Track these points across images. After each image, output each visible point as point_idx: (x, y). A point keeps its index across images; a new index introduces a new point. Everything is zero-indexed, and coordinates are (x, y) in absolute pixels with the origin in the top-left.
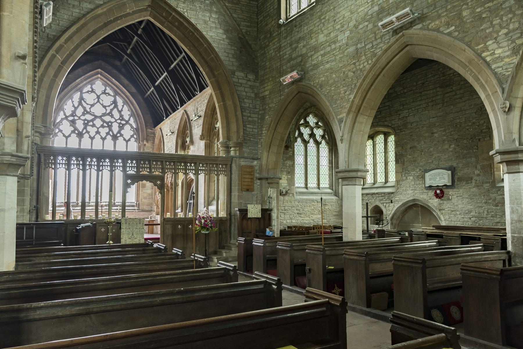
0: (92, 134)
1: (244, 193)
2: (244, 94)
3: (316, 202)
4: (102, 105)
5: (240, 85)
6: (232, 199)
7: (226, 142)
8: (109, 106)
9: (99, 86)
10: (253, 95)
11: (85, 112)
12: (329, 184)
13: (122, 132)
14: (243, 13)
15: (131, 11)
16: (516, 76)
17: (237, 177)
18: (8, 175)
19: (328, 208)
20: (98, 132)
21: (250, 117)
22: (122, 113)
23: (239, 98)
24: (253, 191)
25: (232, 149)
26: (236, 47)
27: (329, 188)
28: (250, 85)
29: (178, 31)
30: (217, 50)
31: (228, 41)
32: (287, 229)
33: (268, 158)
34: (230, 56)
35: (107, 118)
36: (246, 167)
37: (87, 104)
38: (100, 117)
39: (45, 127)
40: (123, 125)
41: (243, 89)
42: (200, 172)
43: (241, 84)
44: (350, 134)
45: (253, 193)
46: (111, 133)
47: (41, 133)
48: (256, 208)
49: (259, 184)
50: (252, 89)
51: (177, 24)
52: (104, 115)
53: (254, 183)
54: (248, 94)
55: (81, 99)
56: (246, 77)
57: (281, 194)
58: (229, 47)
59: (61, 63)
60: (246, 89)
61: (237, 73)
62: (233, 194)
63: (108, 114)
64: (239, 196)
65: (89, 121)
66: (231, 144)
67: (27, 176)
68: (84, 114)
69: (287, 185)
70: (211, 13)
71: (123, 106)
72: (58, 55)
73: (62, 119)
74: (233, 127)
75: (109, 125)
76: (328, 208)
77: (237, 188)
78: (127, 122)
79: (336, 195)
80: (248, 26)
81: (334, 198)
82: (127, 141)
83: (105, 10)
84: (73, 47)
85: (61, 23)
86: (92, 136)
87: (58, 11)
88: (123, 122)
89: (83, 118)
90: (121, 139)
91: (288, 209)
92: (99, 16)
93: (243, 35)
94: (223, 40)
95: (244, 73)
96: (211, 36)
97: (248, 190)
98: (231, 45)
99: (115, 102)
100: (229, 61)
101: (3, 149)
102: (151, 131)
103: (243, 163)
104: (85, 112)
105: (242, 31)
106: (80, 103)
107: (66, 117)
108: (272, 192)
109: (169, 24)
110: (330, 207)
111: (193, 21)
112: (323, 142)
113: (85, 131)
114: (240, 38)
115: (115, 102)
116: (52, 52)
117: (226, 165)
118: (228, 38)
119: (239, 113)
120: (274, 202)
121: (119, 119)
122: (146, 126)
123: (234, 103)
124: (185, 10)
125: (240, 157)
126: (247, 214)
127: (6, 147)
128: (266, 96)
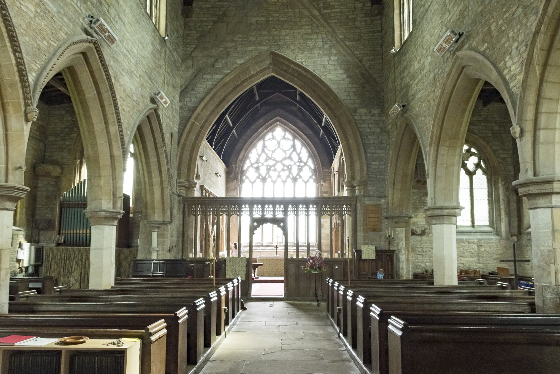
0: (274, 178)
1: (369, 233)
2: (368, 130)
3: (467, 242)
4: (282, 149)
5: (363, 122)
6: (358, 240)
7: (351, 181)
8: (288, 150)
9: (279, 132)
10: (378, 130)
11: (268, 158)
12: (490, 221)
13: (301, 174)
14: (365, 48)
15: (255, 73)
16: (524, 95)
17: (361, 217)
18: (105, 225)
19: (485, 250)
20: (279, 176)
21: (375, 153)
22: (301, 155)
23: (361, 136)
24: (381, 231)
25: (357, 188)
26: (357, 84)
27: (490, 226)
28: (375, 121)
29: (299, 81)
30: (335, 91)
31: (349, 80)
32: (425, 273)
33: (393, 195)
34: (351, 94)
35: (287, 162)
36: (372, 206)
37: (269, 151)
38: (281, 162)
39: (189, 181)
40: (302, 167)
41: (366, 125)
42: (322, 213)
43: (364, 120)
44: (434, 167)
45: (380, 233)
46: (291, 176)
47: (186, 187)
48: (371, 249)
49: (386, 223)
50: (378, 124)
51: (296, 74)
52: (284, 159)
53: (381, 223)
54: (373, 130)
55: (264, 146)
56: (370, 112)
57: (413, 233)
58: (350, 85)
59: (200, 128)
60: (370, 126)
61: (358, 111)
62: (358, 234)
63: (288, 158)
64: (364, 236)
65: (271, 167)
66: (355, 183)
67: (166, 223)
68: (266, 160)
69: (424, 223)
70: (330, 57)
71: (301, 149)
72: (196, 123)
73: (249, 167)
74: (357, 165)
75: (289, 169)
76: (485, 250)
77: (362, 228)
78: (306, 164)
79: (497, 235)
80: (372, 60)
81: (494, 237)
82: (306, 182)
83: (232, 77)
84: (208, 113)
85: (199, 95)
86: (274, 180)
87: (196, 87)
88: (302, 164)
89: (266, 164)
90: (300, 181)
91: (427, 251)
92: (228, 82)
93: (366, 70)
94: (344, 80)
95: (367, 110)
96: (331, 79)
97: (374, 230)
98: (353, 83)
99: (294, 146)
100: (350, 99)
101: (101, 207)
102: (327, 170)
103: (368, 202)
104: (268, 158)
105: (364, 66)
106: (263, 151)
107: (252, 165)
108: (401, 233)
109: (289, 75)
110: (488, 249)
111: (311, 69)
112: (479, 172)
113: (267, 176)
114: (362, 74)
115: (294, 146)
116: (192, 120)
117: (351, 205)
118: (348, 77)
119: (362, 150)
120: (401, 243)
121: (298, 161)
122: (323, 167)
123: (356, 141)
124: (303, 60)
125: (365, 196)
126: (361, 256)
127: (102, 206)
128: (390, 129)
